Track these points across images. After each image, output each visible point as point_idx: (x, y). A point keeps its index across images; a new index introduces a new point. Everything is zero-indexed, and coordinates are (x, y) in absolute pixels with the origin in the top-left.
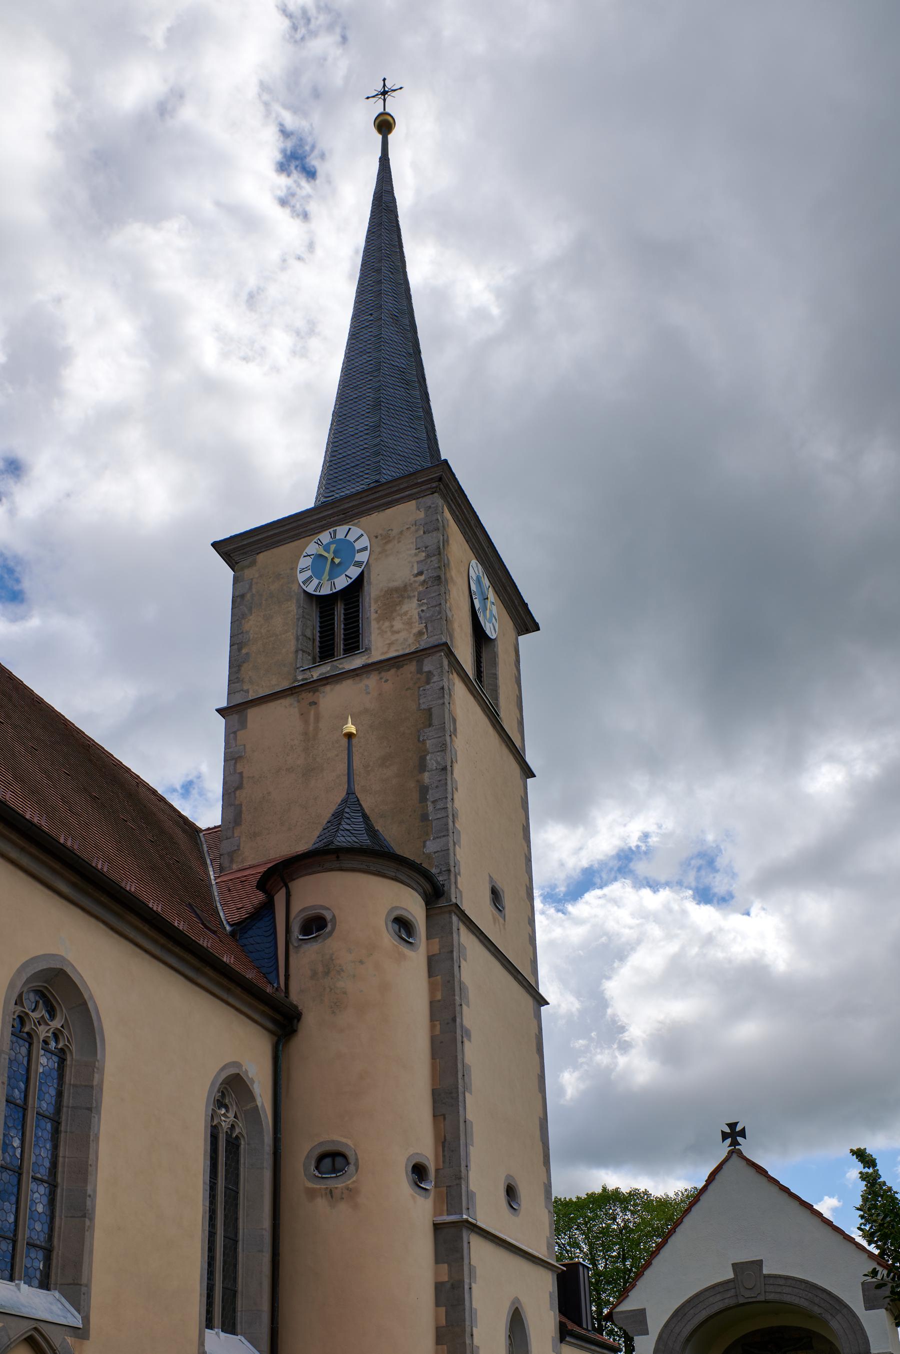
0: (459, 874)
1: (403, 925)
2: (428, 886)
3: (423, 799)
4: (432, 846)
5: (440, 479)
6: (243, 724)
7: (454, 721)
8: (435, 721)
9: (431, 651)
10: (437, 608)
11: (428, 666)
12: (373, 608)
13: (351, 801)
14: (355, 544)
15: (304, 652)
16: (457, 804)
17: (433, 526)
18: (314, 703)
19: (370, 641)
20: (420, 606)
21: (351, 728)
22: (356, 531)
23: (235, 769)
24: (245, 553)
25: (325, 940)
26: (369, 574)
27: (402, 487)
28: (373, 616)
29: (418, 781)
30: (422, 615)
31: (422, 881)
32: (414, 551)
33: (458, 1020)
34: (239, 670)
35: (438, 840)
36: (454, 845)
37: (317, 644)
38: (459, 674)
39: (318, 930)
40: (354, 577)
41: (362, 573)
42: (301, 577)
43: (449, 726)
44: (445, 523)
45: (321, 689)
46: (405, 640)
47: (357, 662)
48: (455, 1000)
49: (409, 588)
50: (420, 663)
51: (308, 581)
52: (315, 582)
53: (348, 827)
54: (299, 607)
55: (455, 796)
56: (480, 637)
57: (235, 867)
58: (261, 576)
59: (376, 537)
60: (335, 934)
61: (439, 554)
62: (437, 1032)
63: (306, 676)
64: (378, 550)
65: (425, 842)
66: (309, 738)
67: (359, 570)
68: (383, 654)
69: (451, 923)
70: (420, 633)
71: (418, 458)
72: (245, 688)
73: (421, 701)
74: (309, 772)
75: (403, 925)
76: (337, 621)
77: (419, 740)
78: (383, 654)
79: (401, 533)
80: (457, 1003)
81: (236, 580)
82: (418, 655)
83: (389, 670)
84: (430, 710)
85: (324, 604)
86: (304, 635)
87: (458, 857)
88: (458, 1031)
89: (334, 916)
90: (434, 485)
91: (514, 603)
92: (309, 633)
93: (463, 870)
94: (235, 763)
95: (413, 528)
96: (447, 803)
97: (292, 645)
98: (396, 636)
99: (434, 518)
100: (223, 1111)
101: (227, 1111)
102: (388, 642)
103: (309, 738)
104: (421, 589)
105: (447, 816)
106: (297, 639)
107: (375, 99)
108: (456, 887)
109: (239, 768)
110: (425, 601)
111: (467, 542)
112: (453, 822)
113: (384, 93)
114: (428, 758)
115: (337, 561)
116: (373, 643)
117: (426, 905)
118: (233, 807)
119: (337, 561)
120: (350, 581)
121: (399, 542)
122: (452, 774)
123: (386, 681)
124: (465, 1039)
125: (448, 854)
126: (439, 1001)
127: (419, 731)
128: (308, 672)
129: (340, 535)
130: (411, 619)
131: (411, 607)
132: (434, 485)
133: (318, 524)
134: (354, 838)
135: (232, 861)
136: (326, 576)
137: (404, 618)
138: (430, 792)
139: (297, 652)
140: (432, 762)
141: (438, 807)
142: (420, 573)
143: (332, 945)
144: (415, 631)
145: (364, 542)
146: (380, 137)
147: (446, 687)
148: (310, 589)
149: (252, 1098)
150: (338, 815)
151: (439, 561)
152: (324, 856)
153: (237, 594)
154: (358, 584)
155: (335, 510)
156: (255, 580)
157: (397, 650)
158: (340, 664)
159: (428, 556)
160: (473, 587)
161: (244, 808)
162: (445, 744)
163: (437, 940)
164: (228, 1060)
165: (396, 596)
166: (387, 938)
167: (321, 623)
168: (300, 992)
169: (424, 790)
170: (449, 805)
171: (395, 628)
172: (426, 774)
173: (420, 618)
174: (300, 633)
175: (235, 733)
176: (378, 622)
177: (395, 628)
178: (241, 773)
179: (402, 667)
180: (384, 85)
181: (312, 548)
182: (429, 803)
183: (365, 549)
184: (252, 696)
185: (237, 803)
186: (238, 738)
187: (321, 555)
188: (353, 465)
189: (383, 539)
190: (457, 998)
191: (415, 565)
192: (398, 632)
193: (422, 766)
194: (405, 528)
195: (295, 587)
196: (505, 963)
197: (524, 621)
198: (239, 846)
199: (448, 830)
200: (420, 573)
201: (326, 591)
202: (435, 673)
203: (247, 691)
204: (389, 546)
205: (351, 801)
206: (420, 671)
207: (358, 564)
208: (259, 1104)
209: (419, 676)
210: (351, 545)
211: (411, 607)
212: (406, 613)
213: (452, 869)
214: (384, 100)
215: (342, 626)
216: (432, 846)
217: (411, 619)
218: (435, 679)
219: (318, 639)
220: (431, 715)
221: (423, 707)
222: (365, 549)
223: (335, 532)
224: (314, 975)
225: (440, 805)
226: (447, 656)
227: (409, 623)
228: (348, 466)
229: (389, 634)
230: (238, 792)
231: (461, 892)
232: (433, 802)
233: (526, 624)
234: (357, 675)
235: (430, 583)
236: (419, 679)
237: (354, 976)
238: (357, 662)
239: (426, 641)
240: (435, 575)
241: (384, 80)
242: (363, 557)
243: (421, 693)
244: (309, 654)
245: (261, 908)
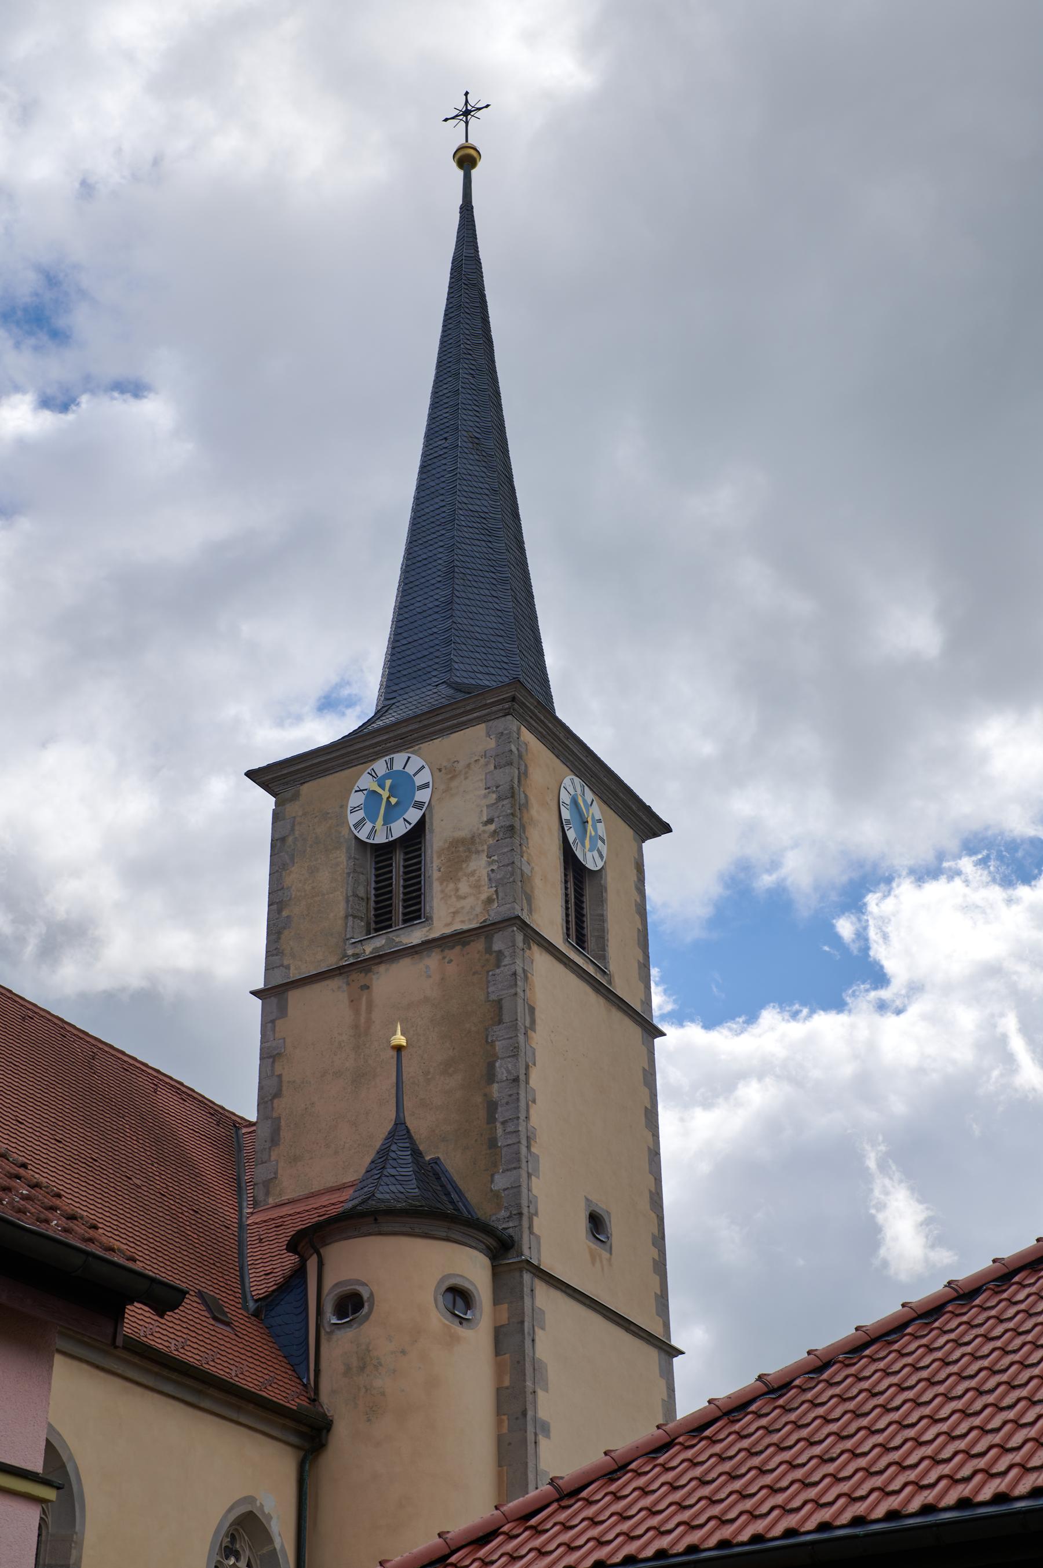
0: (536, 1214)
1: (458, 1298)
2: (491, 1241)
3: (491, 1119)
4: (501, 1182)
5: (513, 699)
6: (283, 1011)
7: (532, 1010)
8: (506, 1018)
9: (502, 925)
10: (509, 868)
11: (498, 944)
12: (436, 863)
13: (400, 1131)
14: (415, 778)
15: (354, 917)
16: (534, 1120)
17: (508, 759)
18: (366, 987)
19: (431, 907)
20: (490, 864)
21: (399, 1039)
22: (416, 762)
23: (273, 1070)
24: (287, 783)
25: (361, 1324)
26: (431, 818)
27: (468, 708)
28: (436, 875)
29: (485, 1095)
30: (492, 875)
31: (482, 1236)
32: (484, 792)
33: (530, 1414)
34: (279, 938)
35: (509, 1173)
36: (529, 1175)
37: (372, 904)
38: (539, 945)
39: (354, 1312)
40: (414, 822)
41: (424, 815)
42: (353, 819)
43: (524, 1020)
44: (523, 750)
45: (375, 968)
46: (472, 908)
47: (415, 936)
48: (525, 1387)
49: (478, 840)
50: (489, 940)
51: (359, 824)
52: (368, 826)
53: (393, 1172)
54: (350, 858)
55: (532, 1111)
56: (575, 871)
57: (271, 1201)
58: (305, 814)
59: (440, 770)
60: (372, 1317)
61: (513, 796)
62: (505, 1430)
63: (357, 951)
64: (442, 787)
65: (492, 1176)
66: (361, 1032)
67: (420, 813)
68: (447, 925)
69: (521, 1283)
70: (489, 901)
71: (501, 639)
72: (286, 963)
73: (490, 989)
74: (360, 1078)
75: (458, 1298)
76: (395, 878)
77: (487, 1041)
78: (447, 925)
79: (469, 766)
80: (529, 1390)
81: (276, 816)
82: (486, 930)
83: (453, 947)
84: (500, 1001)
85: (382, 853)
86: (355, 895)
87: (535, 1191)
88: (530, 1429)
89: (372, 1294)
90: (507, 706)
91: (630, 808)
92: (361, 892)
93: (541, 1207)
94: (273, 1062)
95: (482, 761)
96: (518, 1125)
97: (341, 909)
98: (463, 903)
99: (507, 749)
100: (232, 1561)
101: (237, 1560)
102: (452, 910)
103: (361, 1032)
104: (491, 841)
105: (519, 1142)
106: (347, 901)
107: (455, 121)
108: (531, 1232)
109: (278, 1070)
110: (495, 858)
111: (557, 757)
112: (528, 1147)
113: (467, 113)
114: (497, 1064)
115: (393, 801)
116: (435, 911)
118: (270, 1121)
119: (393, 801)
120: (409, 827)
121: (466, 778)
122: (527, 1082)
123: (450, 961)
124: (540, 1437)
125: (519, 1193)
126: (507, 1388)
127: (487, 1029)
128: (359, 945)
129: (398, 766)
130: (479, 880)
131: (479, 865)
132: (507, 706)
133: (371, 751)
134: (399, 1187)
135: (267, 1194)
136: (380, 821)
137: (471, 879)
138: (500, 1109)
139: (346, 917)
140: (502, 1070)
141: (509, 1130)
142: (490, 821)
143: (371, 1331)
144: (484, 896)
145: (425, 777)
146: (461, 173)
147: (520, 971)
148: (363, 835)
149: (268, 1538)
150: (383, 1155)
151: (513, 806)
152: (363, 1217)
153: (277, 837)
154: (419, 830)
155: (391, 735)
156: (298, 819)
157: (463, 922)
158: (398, 936)
159: (499, 799)
160: (566, 814)
161: (283, 1123)
162: (517, 1048)
163: (506, 1306)
164: (238, 1496)
165: (462, 848)
166: (437, 1319)
167: (377, 876)
168: (334, 1397)
169: (492, 1107)
170: (522, 1128)
171: (461, 892)
172: (495, 1086)
173: (490, 880)
174: (350, 893)
175: (273, 1022)
176: (441, 884)
177: (461, 892)
178: (280, 1076)
179: (468, 943)
180: (467, 102)
181: (366, 782)
182: (498, 1125)
183: (426, 786)
184: (294, 975)
185: (275, 1115)
186: (277, 1029)
187: (374, 792)
188: (419, 655)
189: (448, 774)
190: (529, 1383)
191: (485, 809)
192: (465, 898)
193: (490, 1076)
194: (473, 760)
195: (345, 832)
196: (608, 1314)
197: (651, 825)
198: (276, 1173)
199: (519, 1160)
200: (490, 821)
201: (380, 839)
202: (507, 953)
203: (288, 967)
204: (454, 784)
205: (400, 1131)
206: (488, 950)
207: (419, 805)
208: (278, 1546)
209: (487, 956)
210: (410, 779)
211: (479, 865)
212: (473, 873)
213: (525, 1211)
214: (467, 123)
215: (402, 882)
216: (501, 1182)
217: (479, 880)
218: (506, 961)
219: (373, 898)
220: (501, 1008)
221: (493, 997)
222: (426, 786)
223: (392, 760)
224: (348, 1371)
225: (511, 1128)
226: (521, 929)
227: (477, 886)
228: (413, 657)
229: (454, 899)
230: (275, 1101)
231: (538, 1238)
232: (503, 1123)
233: (652, 829)
234: (416, 953)
235: (501, 835)
236: (487, 960)
237: (394, 1371)
238: (415, 936)
239: (496, 912)
240: (508, 823)
241: (467, 94)
242: (423, 796)
243: (490, 978)
244: (361, 919)
245: (290, 1277)
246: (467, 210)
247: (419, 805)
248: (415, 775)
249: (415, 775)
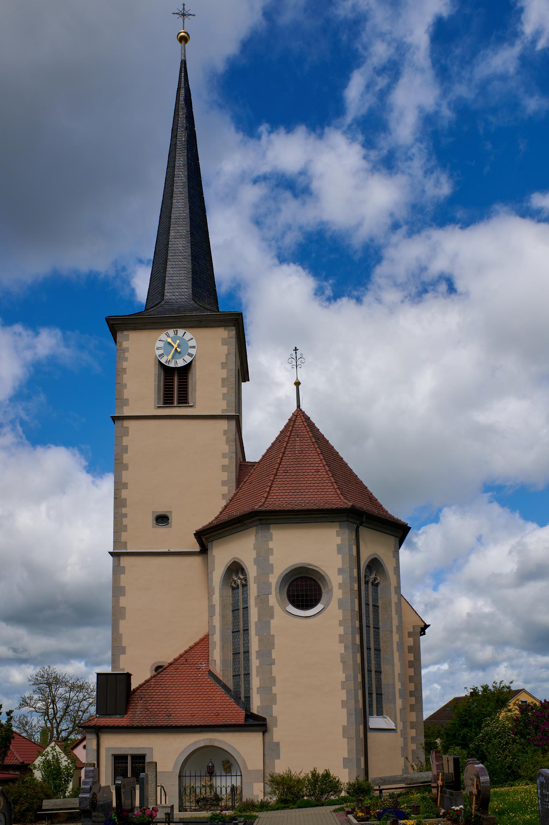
40: (188, 362)
107: (189, 12)
117: (115, 760)
120: (186, 364)
145: (193, 343)
148: (163, 361)
154: (188, 368)
183: (194, 347)
201: (172, 365)
207: (190, 355)
210: (186, 342)
222: (194, 347)
223: (177, 331)
242: (193, 351)
246: (184, 64)
247: (190, 355)
248: (188, 341)
249: (188, 341)
